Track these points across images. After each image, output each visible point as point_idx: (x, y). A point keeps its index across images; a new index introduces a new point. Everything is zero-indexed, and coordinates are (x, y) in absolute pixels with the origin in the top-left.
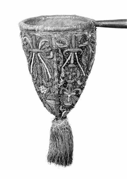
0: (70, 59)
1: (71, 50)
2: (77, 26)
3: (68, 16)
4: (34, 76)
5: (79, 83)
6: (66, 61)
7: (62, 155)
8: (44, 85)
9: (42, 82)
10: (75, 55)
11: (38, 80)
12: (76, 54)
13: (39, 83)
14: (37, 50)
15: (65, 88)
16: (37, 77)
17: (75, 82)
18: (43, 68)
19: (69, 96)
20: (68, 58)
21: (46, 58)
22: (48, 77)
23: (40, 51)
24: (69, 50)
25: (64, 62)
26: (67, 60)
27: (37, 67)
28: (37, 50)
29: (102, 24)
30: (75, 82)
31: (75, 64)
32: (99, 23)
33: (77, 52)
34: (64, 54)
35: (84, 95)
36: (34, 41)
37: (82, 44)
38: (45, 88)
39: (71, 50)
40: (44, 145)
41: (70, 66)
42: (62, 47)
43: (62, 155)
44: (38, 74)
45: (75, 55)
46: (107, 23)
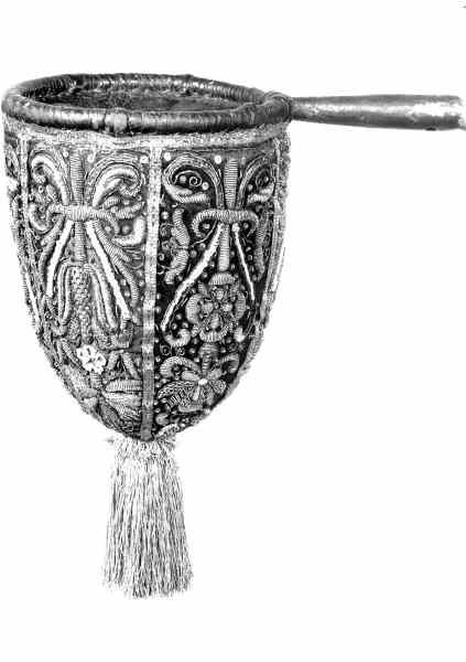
0: (218, 249)
1: (221, 214)
2: (243, 116)
3: (166, 77)
4: (59, 309)
5: (240, 337)
6: (200, 256)
7: (154, 556)
8: (98, 344)
9: (91, 331)
10: (232, 234)
11: (74, 325)
12: (236, 228)
13: (80, 335)
14: (86, 210)
15: (192, 360)
16: (71, 312)
17: (230, 335)
18: (94, 281)
19: (203, 382)
20: (208, 242)
21: (115, 245)
22: (117, 313)
23: (95, 212)
24: (211, 213)
25: (192, 263)
26: (208, 255)
27: (71, 278)
28: (86, 210)
29: (317, 112)
30: (230, 335)
31: (232, 273)
32: (308, 106)
33: (241, 224)
34: (195, 228)
35: (246, 380)
36: (76, 176)
37: (258, 192)
38: (99, 355)
39: (221, 214)
40: (90, 536)
41: (217, 279)
42: (186, 200)
43: (154, 556)
44: (73, 303)
45: (232, 234)
46: (335, 109)
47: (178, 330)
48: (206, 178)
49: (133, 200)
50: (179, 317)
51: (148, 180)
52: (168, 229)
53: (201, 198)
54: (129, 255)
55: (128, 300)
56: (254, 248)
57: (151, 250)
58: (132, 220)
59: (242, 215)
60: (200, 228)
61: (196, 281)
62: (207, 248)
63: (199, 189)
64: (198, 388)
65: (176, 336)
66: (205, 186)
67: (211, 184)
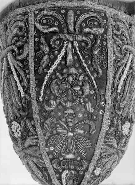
1: (66, 37)
10: (74, 47)
12: (76, 44)
25: (52, 61)
26: (59, 58)
45: (74, 47)
47: (49, 100)
48: (57, 19)
49: (23, 36)
50: (48, 92)
51: (28, 25)
52: (38, 46)
53: (54, 29)
54: (22, 63)
55: (23, 87)
56: (92, 58)
57: (31, 61)
58: (23, 45)
59: (80, 38)
60: (55, 44)
61: (54, 71)
62: (59, 53)
63: (53, 26)
64: (70, 141)
65: (50, 105)
66: (56, 24)
67: (60, 22)
